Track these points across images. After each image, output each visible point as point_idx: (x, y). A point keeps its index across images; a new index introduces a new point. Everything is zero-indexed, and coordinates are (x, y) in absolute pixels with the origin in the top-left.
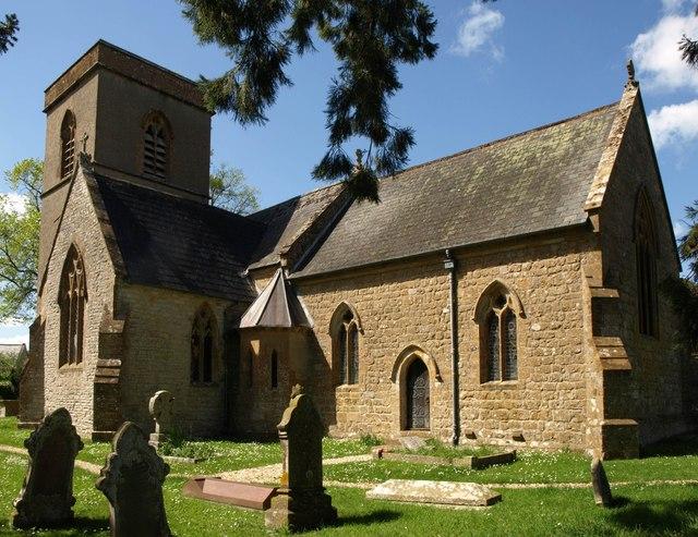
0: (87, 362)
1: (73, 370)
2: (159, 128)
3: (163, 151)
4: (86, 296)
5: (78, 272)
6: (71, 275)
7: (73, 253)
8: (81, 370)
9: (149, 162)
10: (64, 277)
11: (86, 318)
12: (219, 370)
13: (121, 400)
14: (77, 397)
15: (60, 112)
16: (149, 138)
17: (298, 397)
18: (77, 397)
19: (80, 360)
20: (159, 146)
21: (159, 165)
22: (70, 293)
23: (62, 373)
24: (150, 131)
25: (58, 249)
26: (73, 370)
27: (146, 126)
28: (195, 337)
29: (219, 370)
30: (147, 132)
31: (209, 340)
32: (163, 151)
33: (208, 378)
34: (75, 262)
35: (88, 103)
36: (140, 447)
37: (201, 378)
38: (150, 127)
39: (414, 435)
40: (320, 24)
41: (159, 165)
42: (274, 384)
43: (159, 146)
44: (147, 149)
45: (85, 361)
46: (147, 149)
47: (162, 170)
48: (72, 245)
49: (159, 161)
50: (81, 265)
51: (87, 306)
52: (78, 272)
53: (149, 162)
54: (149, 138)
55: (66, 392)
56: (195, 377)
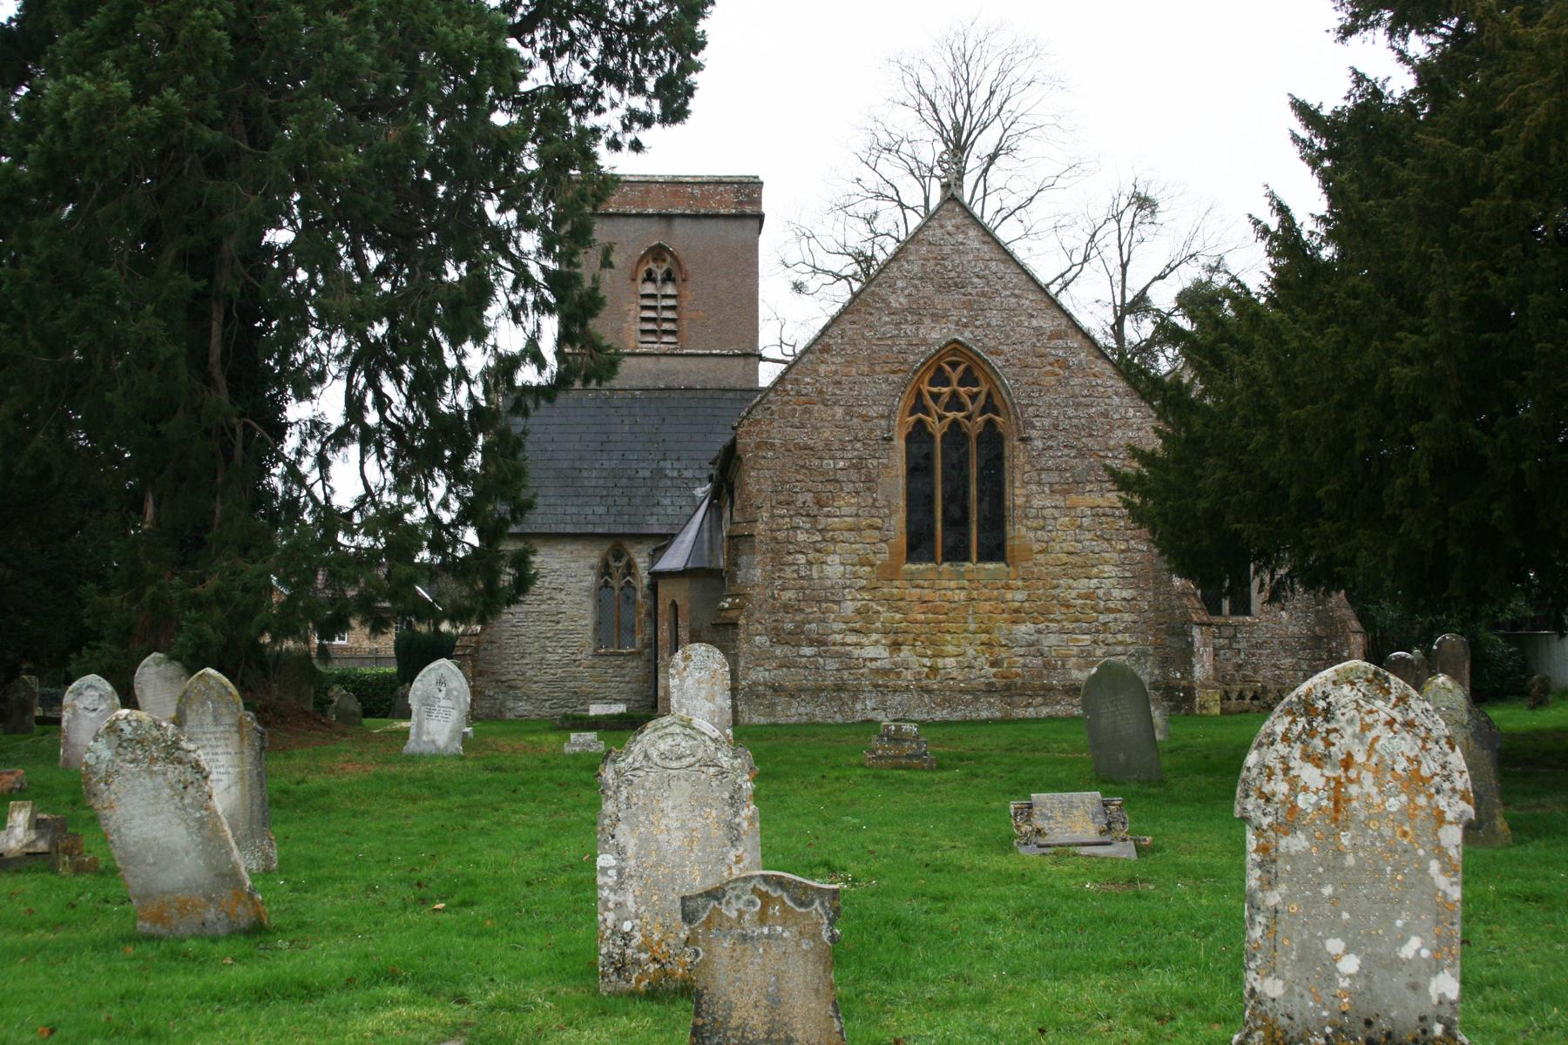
9: (650, 326)
16: (649, 288)
41: (666, 326)
53: (650, 326)
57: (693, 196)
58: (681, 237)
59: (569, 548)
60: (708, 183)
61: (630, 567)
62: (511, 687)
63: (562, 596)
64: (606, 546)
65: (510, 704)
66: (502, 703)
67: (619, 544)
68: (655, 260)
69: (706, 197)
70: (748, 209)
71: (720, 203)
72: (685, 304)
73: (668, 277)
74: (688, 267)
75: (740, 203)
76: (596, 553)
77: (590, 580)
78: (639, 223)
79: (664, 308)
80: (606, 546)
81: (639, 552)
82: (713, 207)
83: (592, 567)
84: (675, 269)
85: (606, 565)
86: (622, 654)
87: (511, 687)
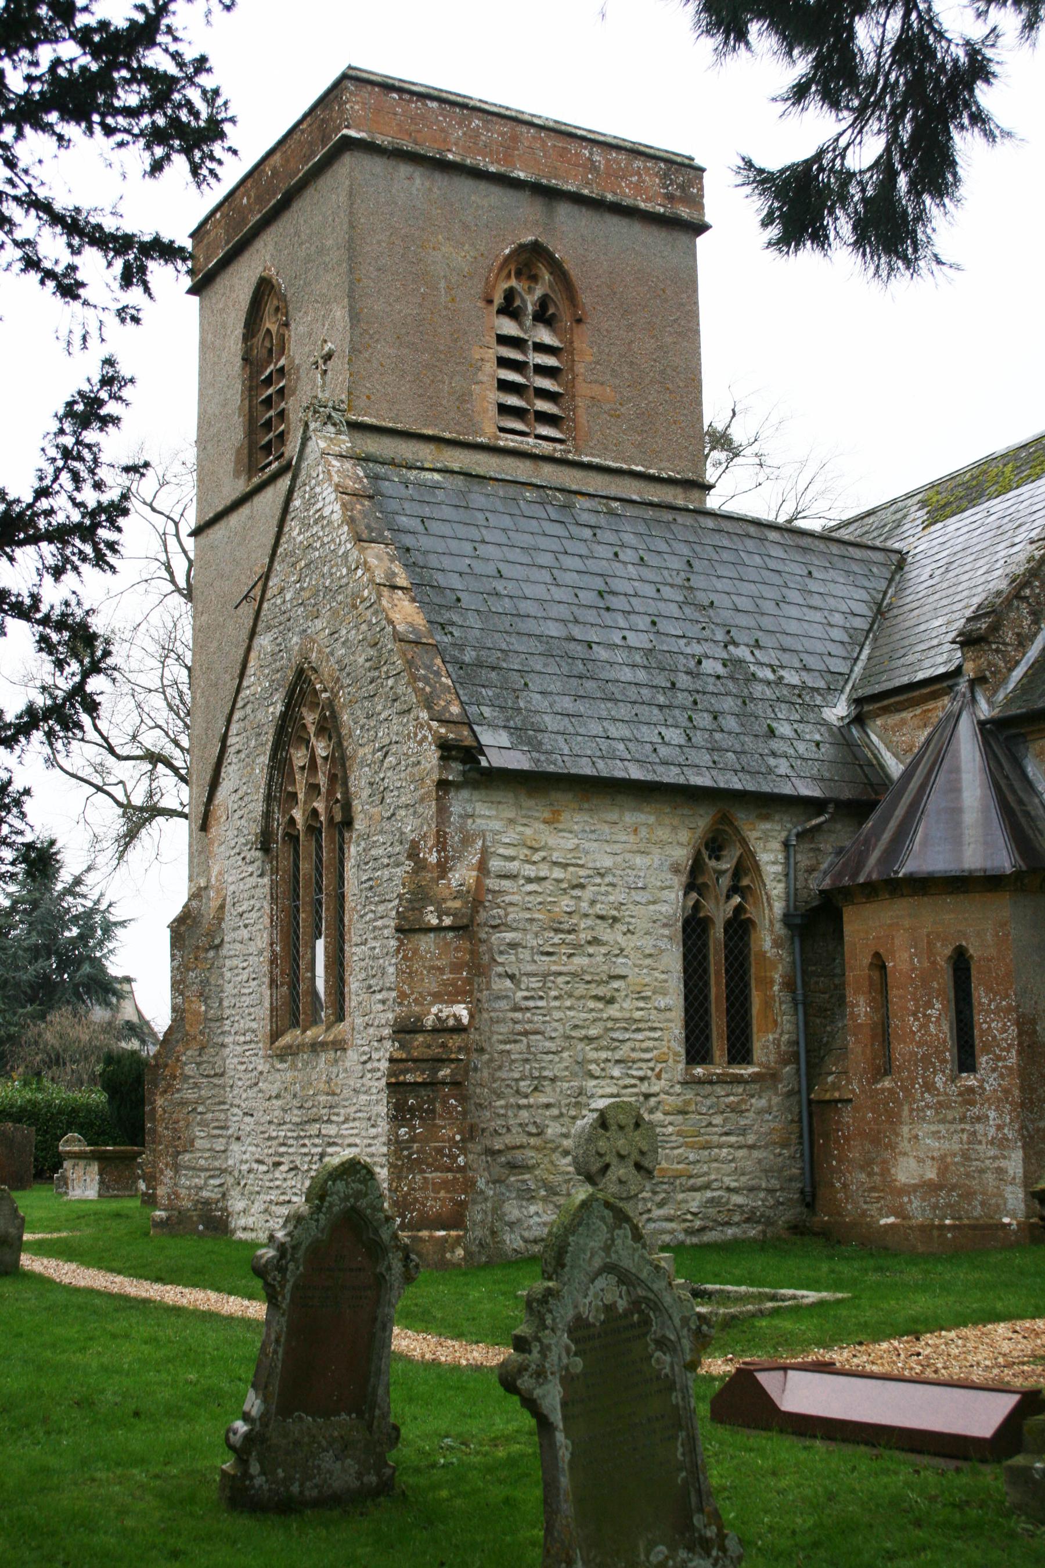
0: (359, 1021)
1: (316, 1047)
2: (539, 292)
3: (550, 361)
4: (348, 823)
5: (321, 749)
6: (299, 757)
7: (299, 687)
8: (340, 1046)
9: (513, 401)
10: (279, 765)
11: (351, 887)
12: (772, 1035)
13: (471, 1133)
14: (331, 1130)
15: (238, 285)
16: (509, 327)
17: (756, 1069)
18: (331, 1130)
19: (340, 1016)
20: (541, 348)
21: (542, 405)
22: (298, 814)
23: (282, 1058)
24: (510, 309)
25: (255, 684)
26: (316, 1047)
27: (498, 299)
28: (694, 929)
29: (772, 1035)
30: (501, 311)
31: (740, 927)
32: (550, 361)
33: (740, 1050)
34: (310, 718)
35: (321, 251)
36: (626, 1263)
37: (719, 1048)
38: (510, 295)
39: (350, 921)
40: (1029, 19)
41: (542, 405)
42: (966, 1062)
43: (541, 348)
44: (503, 363)
45: (355, 1019)
46: (503, 363)
47: (551, 420)
48: (300, 672)
49: (542, 394)
50: (329, 727)
51: (353, 851)
52: (321, 749)
53: (513, 401)
54: (509, 327)
55: (295, 1116)
56: (697, 1049)
57: (593, 168)
58: (571, 235)
59: (630, 818)
60: (618, 148)
61: (747, 865)
62: (513, 1167)
63: (612, 936)
64: (702, 821)
65: (512, 1211)
66: (497, 1210)
67: (725, 819)
68: (519, 275)
69: (617, 175)
70: (684, 212)
71: (638, 187)
72: (580, 368)
73: (543, 316)
74: (585, 298)
75: (670, 197)
76: (684, 836)
77: (672, 901)
78: (496, 196)
79: (540, 370)
80: (702, 821)
81: (766, 837)
82: (625, 194)
83: (676, 870)
84: (557, 297)
85: (697, 868)
86: (738, 1080)
87: (513, 1167)
